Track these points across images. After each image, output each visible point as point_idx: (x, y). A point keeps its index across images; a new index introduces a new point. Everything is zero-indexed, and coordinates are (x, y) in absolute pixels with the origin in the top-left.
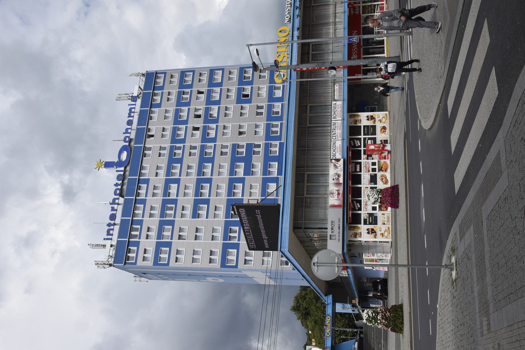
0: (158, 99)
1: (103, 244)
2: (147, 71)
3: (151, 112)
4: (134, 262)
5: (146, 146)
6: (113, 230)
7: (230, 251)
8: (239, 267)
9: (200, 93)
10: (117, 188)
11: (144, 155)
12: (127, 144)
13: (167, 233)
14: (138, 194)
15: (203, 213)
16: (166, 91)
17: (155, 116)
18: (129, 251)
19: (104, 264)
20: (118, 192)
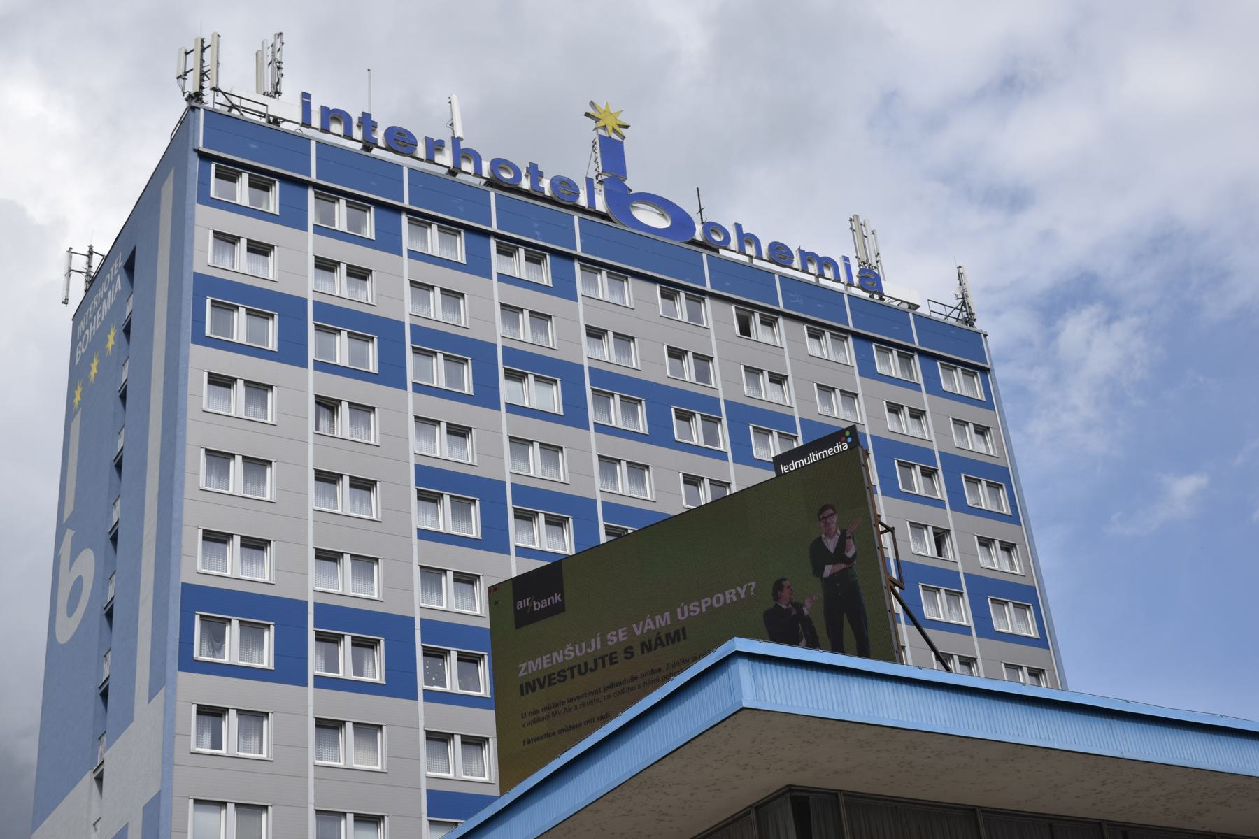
0: (890, 365)
1: (283, 87)
2: (985, 336)
3: (840, 334)
4: (212, 194)
5: (708, 300)
6: (348, 135)
7: (266, 634)
8: (185, 678)
9: (940, 537)
10: (524, 172)
11: (670, 291)
12: (698, 236)
13: (342, 349)
14: (508, 246)
15: (443, 518)
16: (925, 401)
17: (825, 348)
18: (261, 182)
19: (203, 74)
20: (506, 176)
